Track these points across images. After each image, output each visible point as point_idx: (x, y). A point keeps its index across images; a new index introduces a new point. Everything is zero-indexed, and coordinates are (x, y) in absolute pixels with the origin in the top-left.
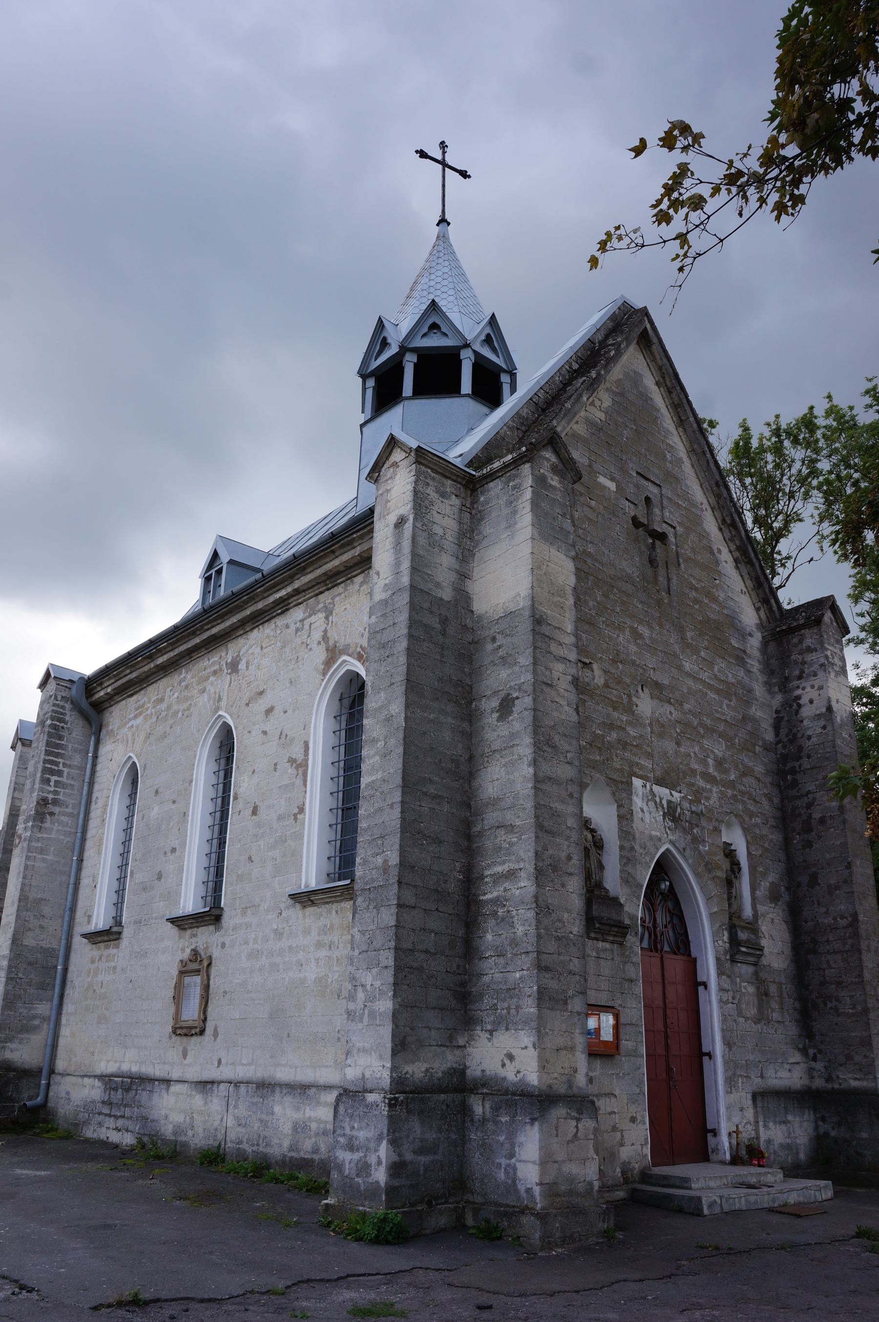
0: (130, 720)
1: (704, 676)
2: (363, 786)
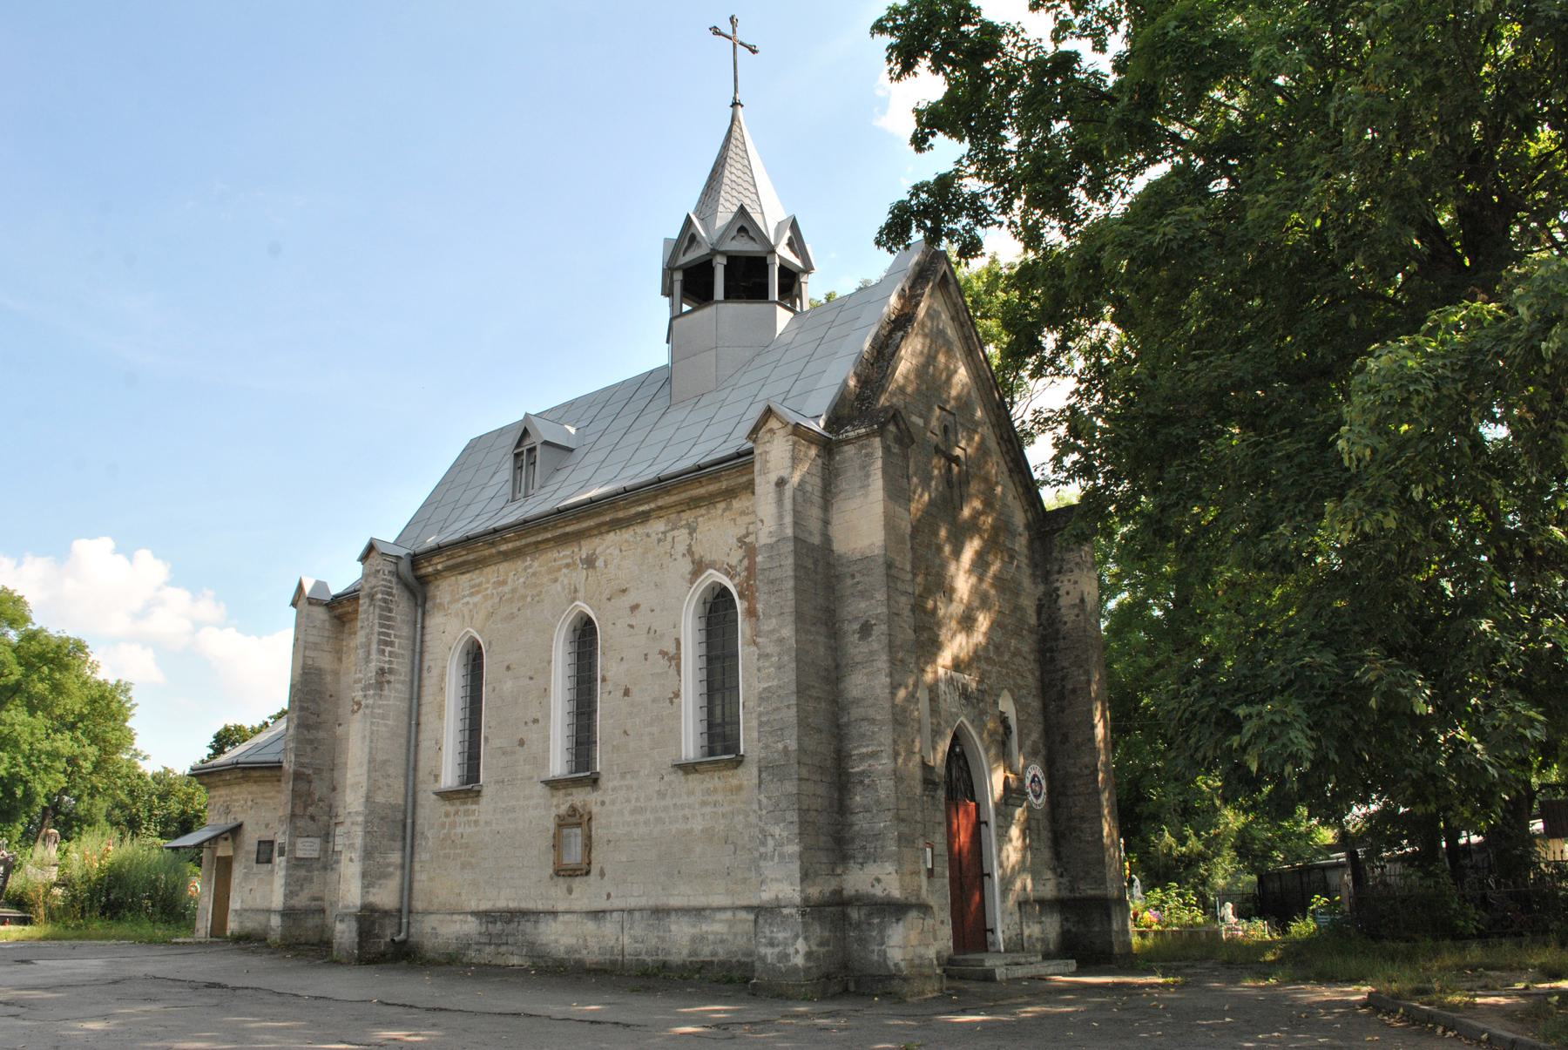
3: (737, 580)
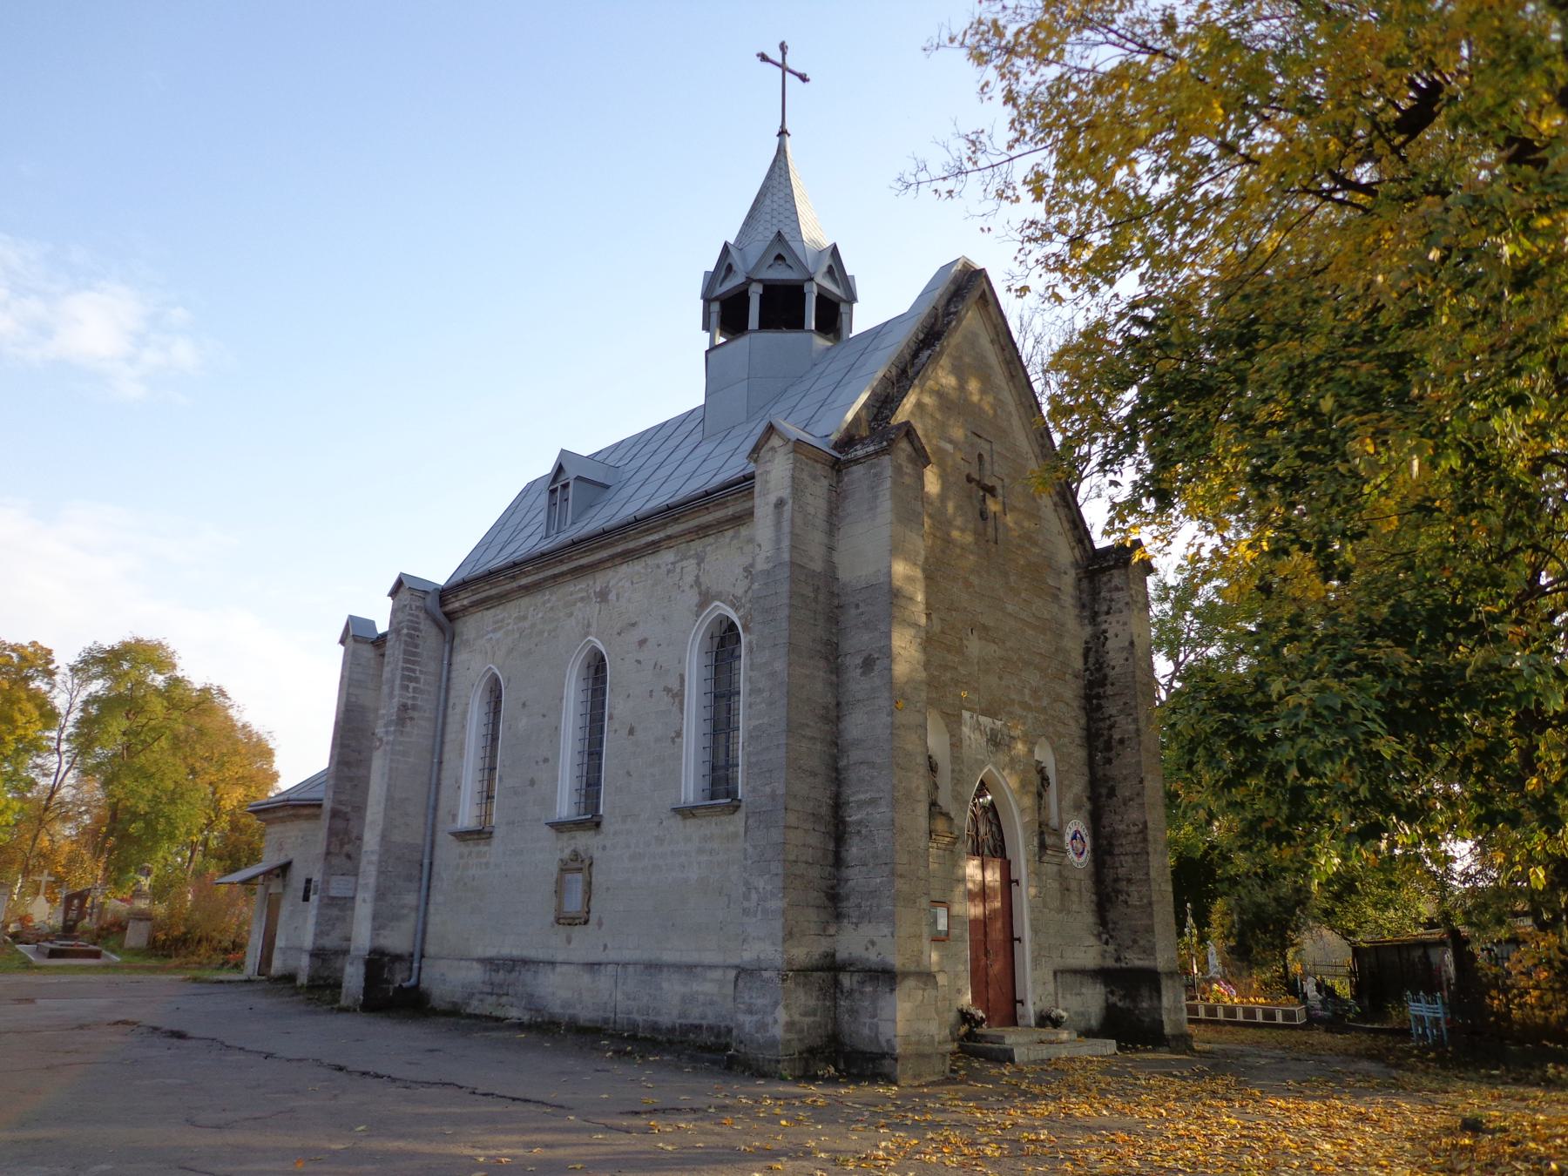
1: (1023, 615)
3: (741, 612)
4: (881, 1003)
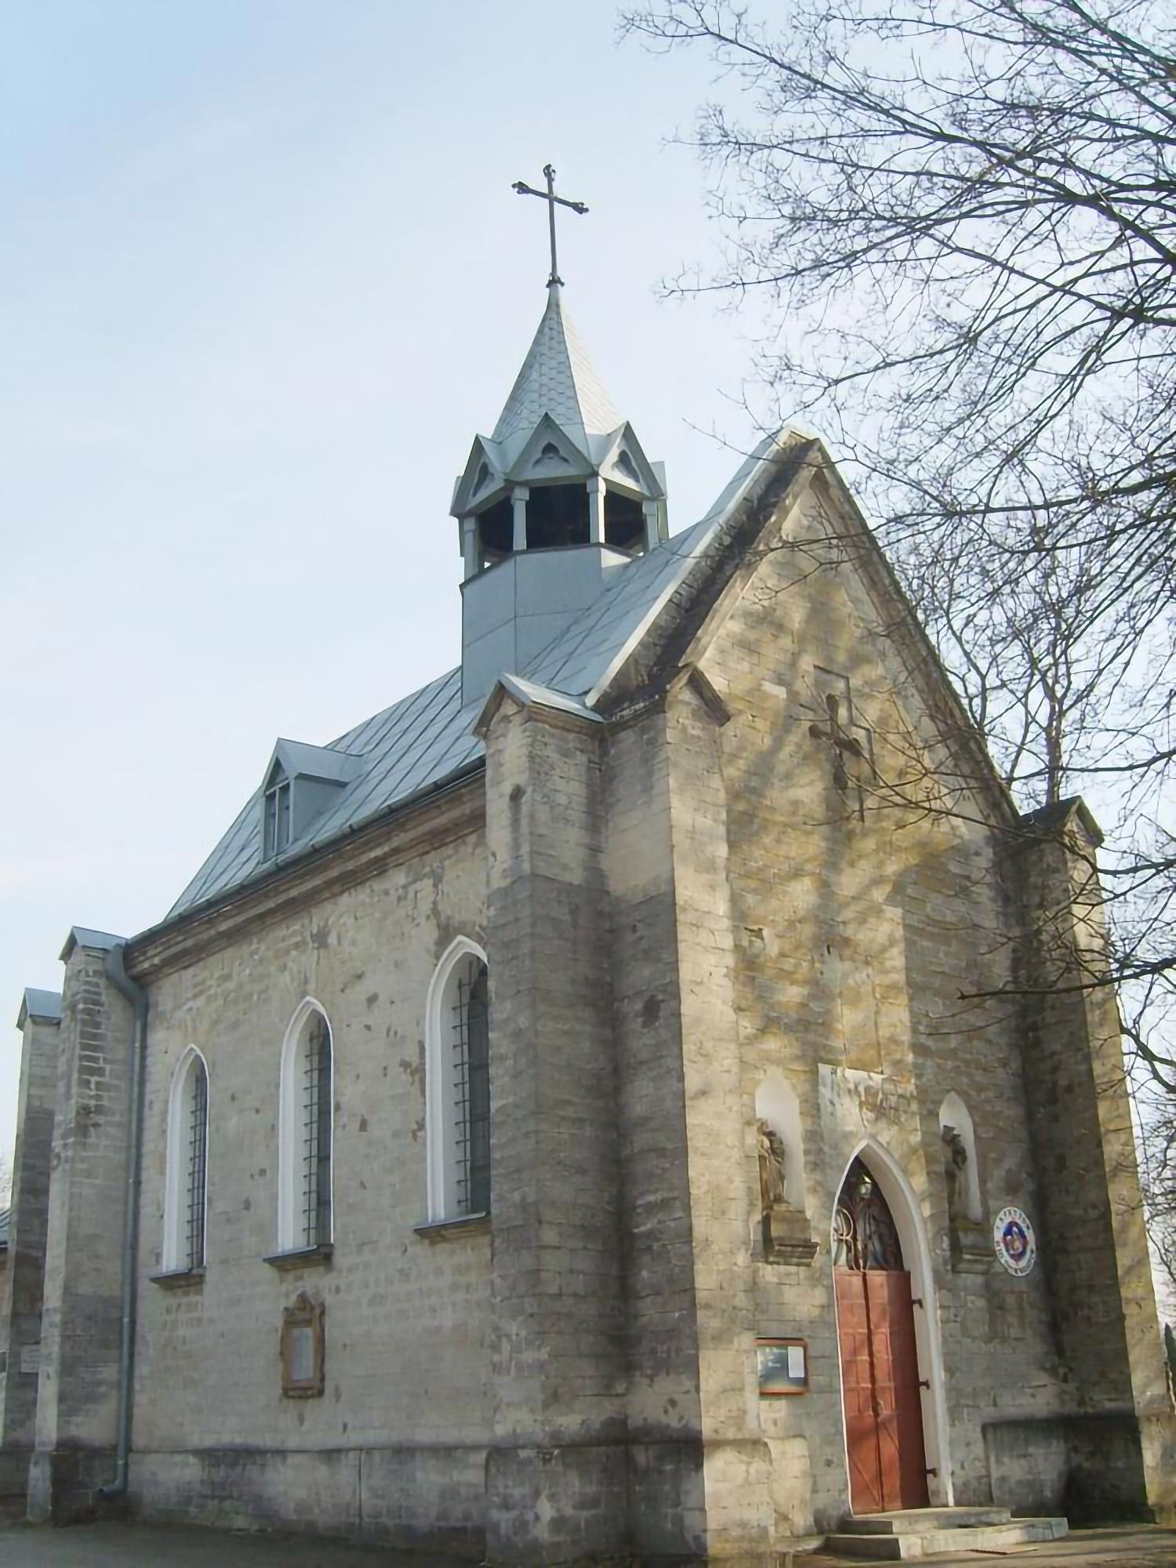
0: (188, 1000)
2: (493, 1110)
4: (687, 1486)
